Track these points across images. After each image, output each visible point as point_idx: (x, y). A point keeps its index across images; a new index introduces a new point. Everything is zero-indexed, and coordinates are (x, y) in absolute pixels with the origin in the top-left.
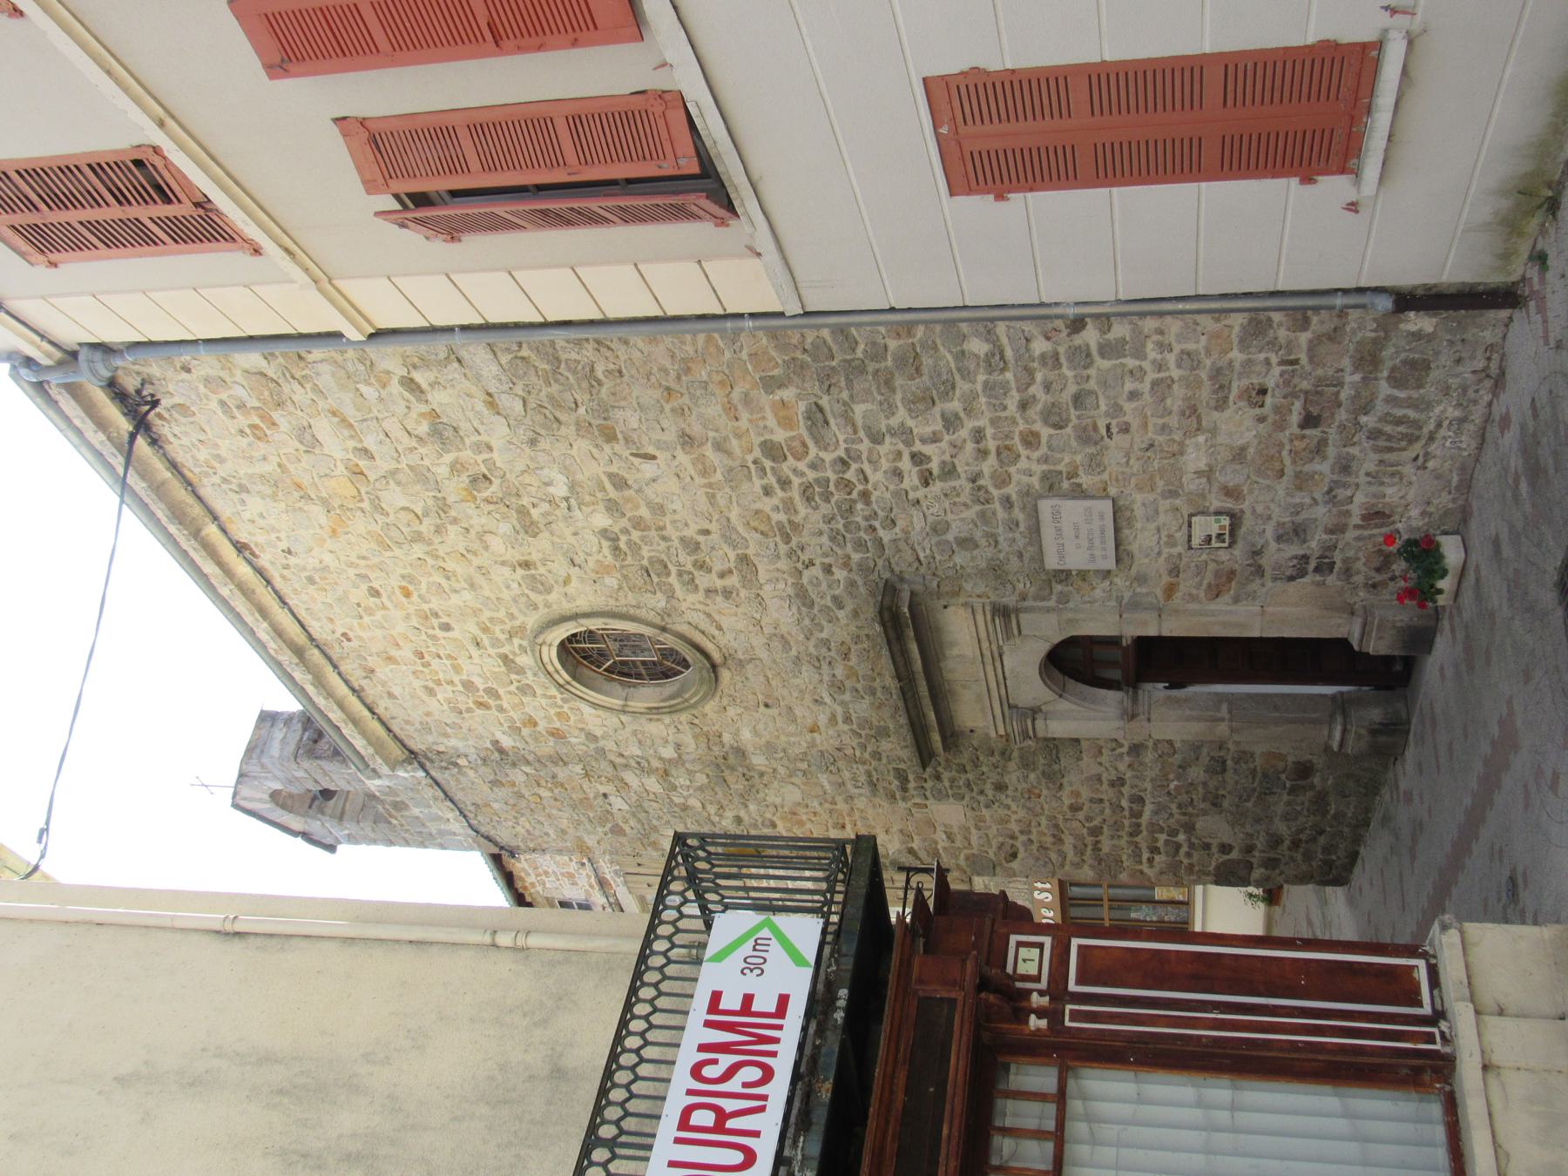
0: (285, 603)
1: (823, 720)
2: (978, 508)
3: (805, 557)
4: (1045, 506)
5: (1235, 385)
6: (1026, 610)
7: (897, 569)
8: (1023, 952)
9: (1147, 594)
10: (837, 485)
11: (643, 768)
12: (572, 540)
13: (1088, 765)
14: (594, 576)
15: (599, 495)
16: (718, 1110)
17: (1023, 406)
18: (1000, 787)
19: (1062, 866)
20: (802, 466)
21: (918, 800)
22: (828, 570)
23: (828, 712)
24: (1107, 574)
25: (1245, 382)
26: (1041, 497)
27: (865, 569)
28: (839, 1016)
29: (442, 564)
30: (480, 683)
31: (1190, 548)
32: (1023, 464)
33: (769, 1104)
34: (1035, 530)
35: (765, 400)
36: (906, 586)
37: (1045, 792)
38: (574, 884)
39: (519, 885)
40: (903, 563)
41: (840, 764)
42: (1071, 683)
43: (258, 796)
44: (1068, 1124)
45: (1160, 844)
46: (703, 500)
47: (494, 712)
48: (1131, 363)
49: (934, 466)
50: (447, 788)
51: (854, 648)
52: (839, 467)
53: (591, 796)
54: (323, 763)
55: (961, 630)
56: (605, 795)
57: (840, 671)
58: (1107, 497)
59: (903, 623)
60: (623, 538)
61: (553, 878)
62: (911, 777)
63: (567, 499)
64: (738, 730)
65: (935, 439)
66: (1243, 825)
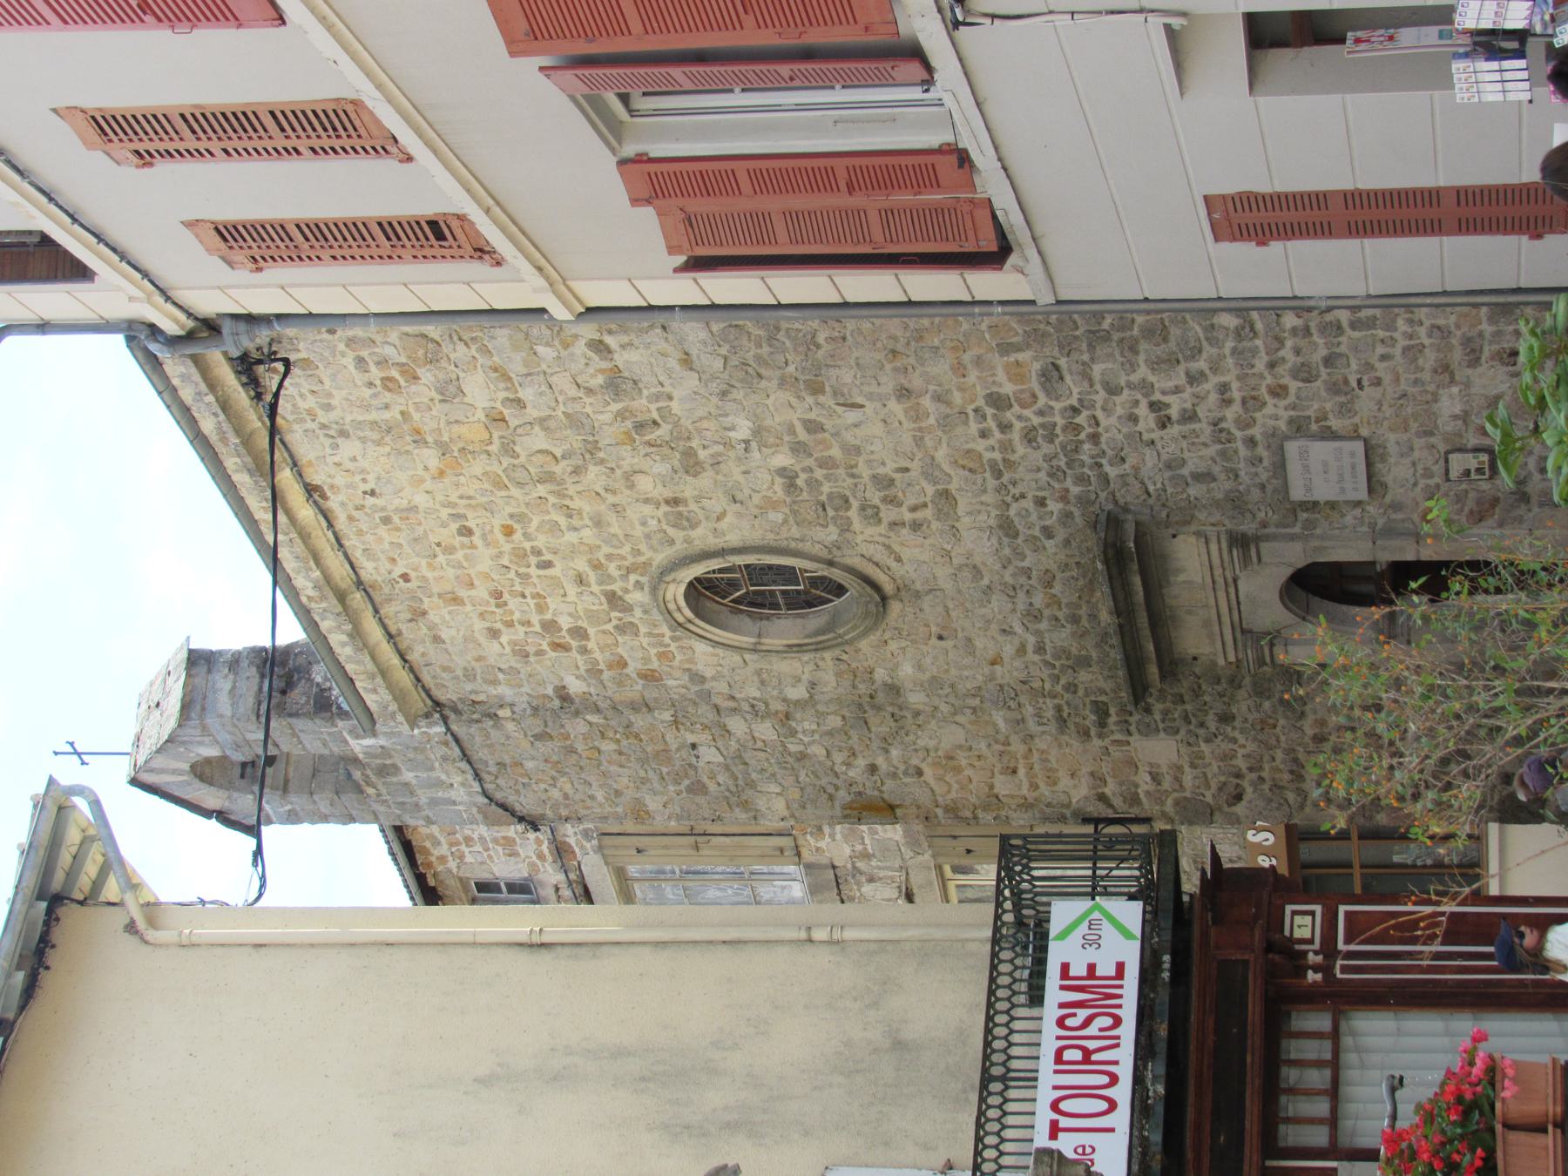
0: (341, 545)
1: (1009, 650)
2: (1219, 447)
3: (1016, 491)
4: (1292, 447)
5: (1486, 349)
6: (1268, 538)
7: (1121, 502)
8: (1298, 919)
9: (1403, 521)
10: (1064, 430)
11: (756, 711)
12: (741, 478)
14: (756, 511)
15: (787, 438)
16: (1084, 1049)
17: (1272, 365)
18: (1226, 718)
19: (1302, 807)
20: (1027, 413)
21: (1118, 736)
22: (1041, 502)
23: (1016, 641)
24: (1358, 503)
25: (1495, 347)
26: (1287, 438)
27: (1083, 501)
28: (1166, 975)
29: (567, 502)
30: (565, 622)
31: (1448, 480)
32: (1269, 410)
33: (1122, 1042)
34: (1280, 466)
35: (999, 362)
36: (1130, 517)
37: (1282, 722)
38: (513, 854)
39: (420, 859)
40: (1130, 496)
41: (1023, 699)
42: (1316, 601)
43: (174, 771)
44: (1342, 1055)
46: (907, 438)
47: (574, 653)
48: (1381, 333)
49: (1174, 412)
50: (466, 745)
51: (1059, 576)
52: (1069, 413)
53: (674, 747)
54: (299, 724)
55: (1191, 560)
56: (694, 746)
57: (1038, 600)
58: (1359, 437)
59: (1126, 555)
60: (803, 476)
61: (478, 848)
62: (1112, 711)
63: (747, 442)
64: (897, 665)
65: (1177, 390)
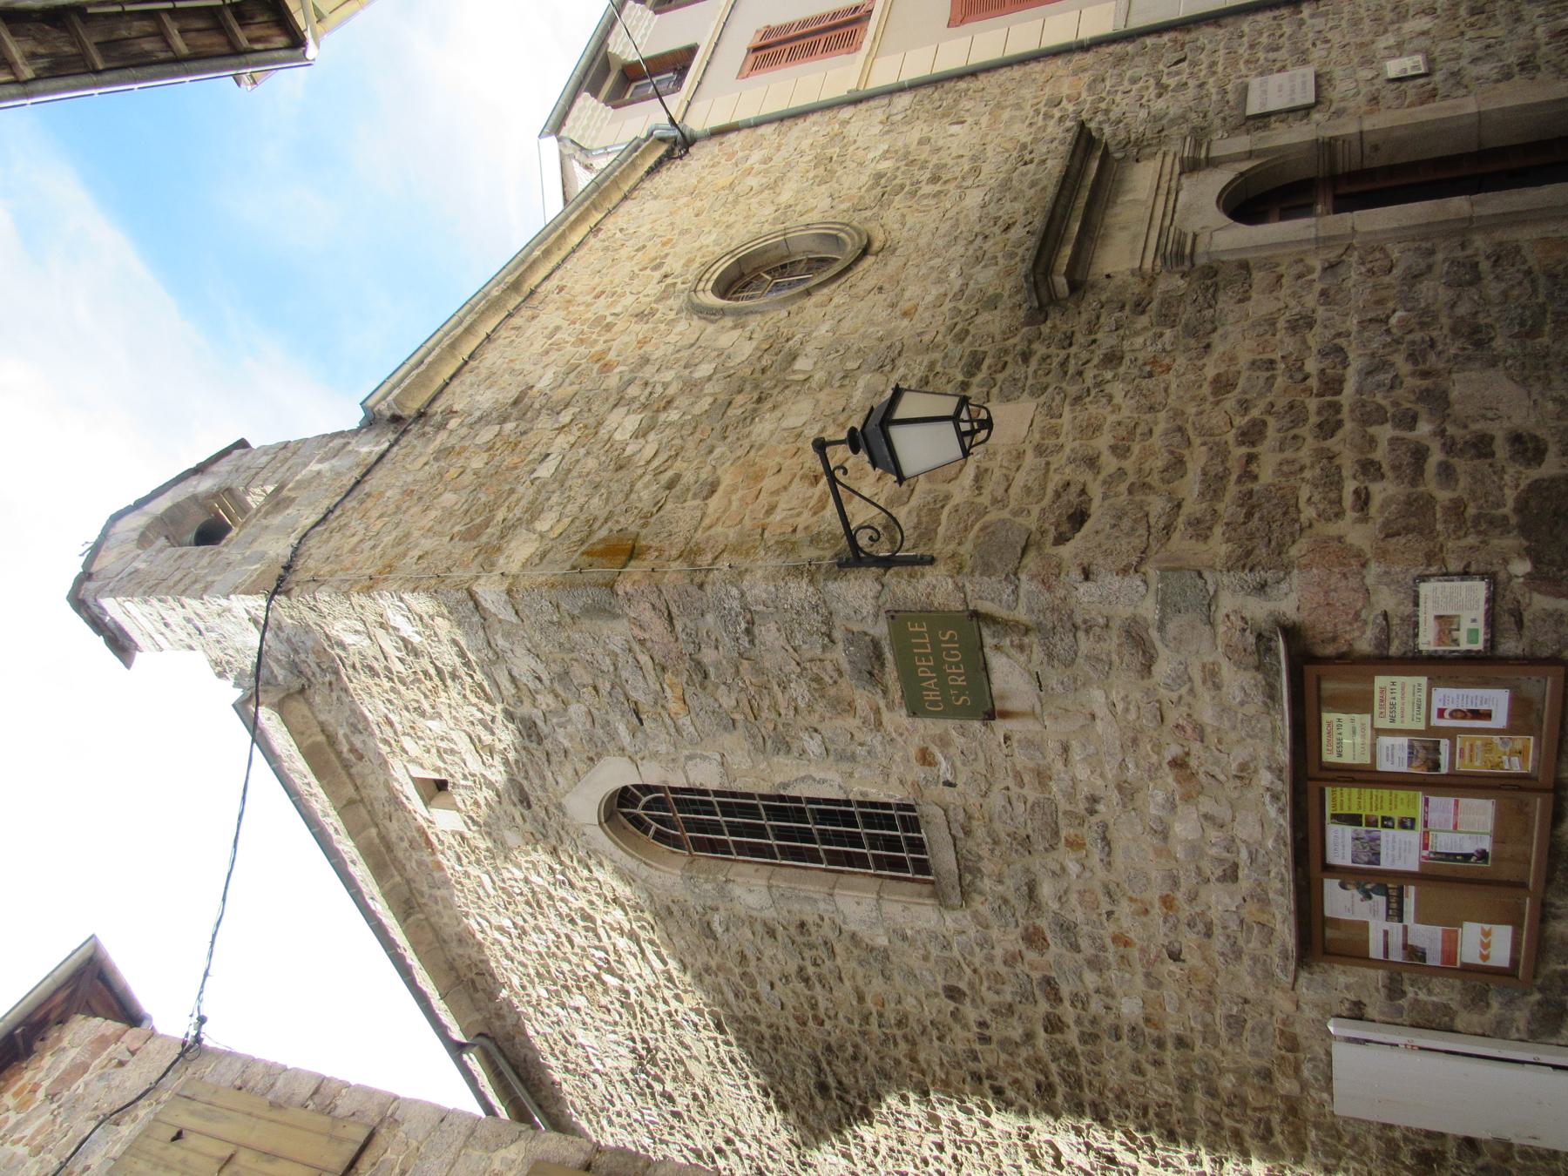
13: (1261, 305)
45: (1381, 454)
66: (1547, 382)
